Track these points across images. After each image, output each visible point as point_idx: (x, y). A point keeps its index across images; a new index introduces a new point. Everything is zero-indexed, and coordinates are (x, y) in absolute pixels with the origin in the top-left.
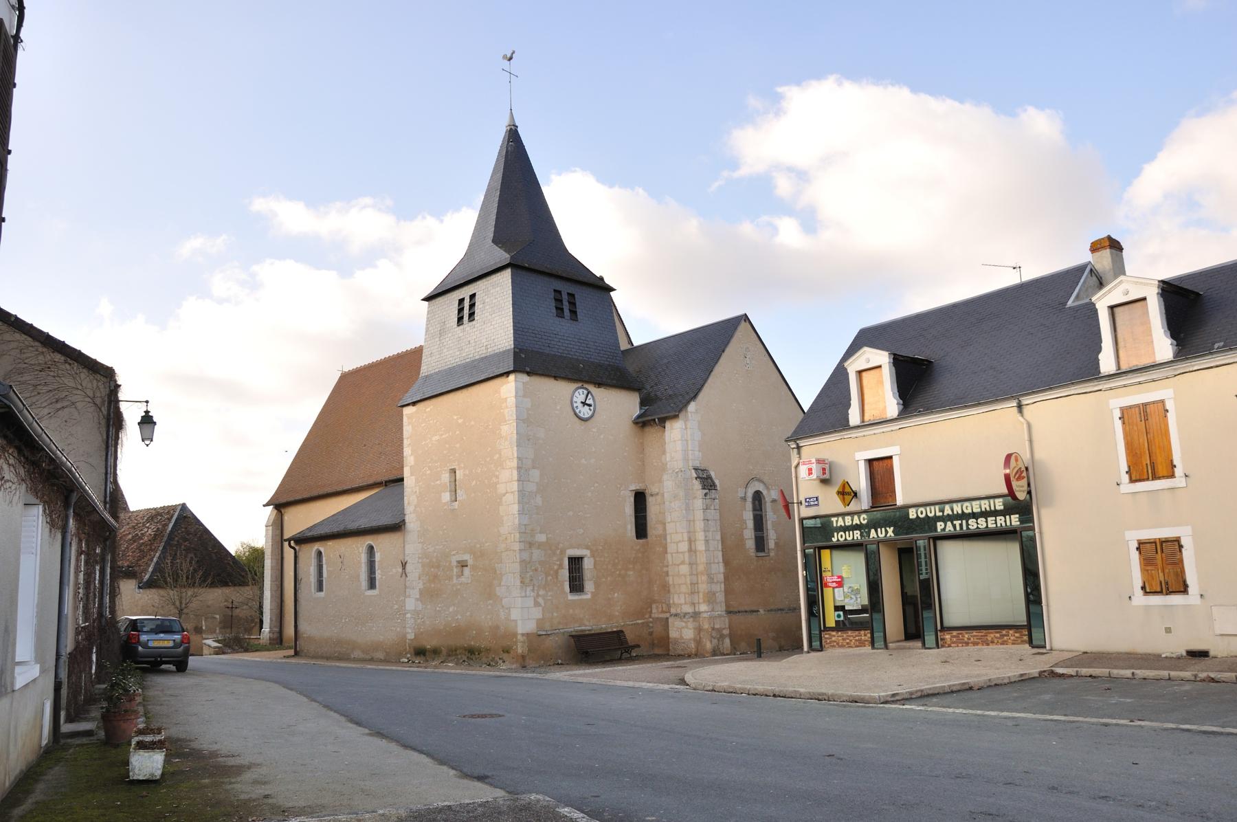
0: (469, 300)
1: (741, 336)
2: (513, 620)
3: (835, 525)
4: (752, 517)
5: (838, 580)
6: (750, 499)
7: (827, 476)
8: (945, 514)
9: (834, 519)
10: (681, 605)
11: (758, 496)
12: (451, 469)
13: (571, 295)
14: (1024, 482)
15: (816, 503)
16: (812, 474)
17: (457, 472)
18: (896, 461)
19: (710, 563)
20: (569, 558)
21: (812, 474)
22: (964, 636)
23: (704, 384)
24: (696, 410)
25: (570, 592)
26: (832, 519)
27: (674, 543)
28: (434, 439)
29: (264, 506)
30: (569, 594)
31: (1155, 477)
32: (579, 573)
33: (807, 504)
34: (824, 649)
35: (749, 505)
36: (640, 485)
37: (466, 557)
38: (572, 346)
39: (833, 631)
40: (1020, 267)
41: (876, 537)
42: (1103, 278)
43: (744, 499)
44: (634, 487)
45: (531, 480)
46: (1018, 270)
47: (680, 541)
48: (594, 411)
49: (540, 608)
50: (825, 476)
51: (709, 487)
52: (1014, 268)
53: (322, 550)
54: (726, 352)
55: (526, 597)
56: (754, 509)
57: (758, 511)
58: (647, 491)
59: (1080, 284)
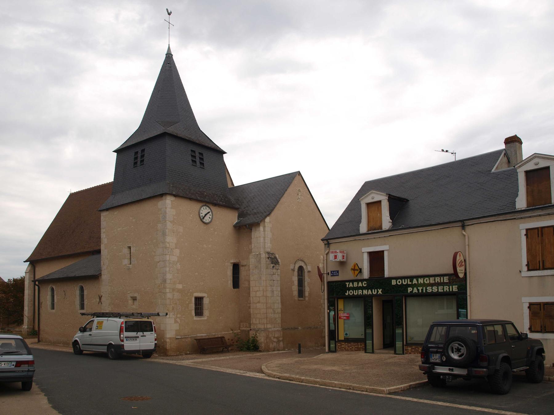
0: (140, 153)
1: (296, 183)
2: (162, 330)
3: (347, 286)
4: (297, 279)
5: (347, 315)
6: (296, 270)
7: (344, 260)
8: (413, 283)
9: (347, 284)
10: (257, 324)
11: (301, 269)
12: (128, 247)
13: (201, 154)
14: (463, 268)
15: (337, 274)
16: (336, 258)
17: (131, 248)
18: (386, 254)
19: (274, 303)
20: (195, 298)
21: (336, 258)
22: (419, 349)
23: (275, 207)
24: (270, 221)
25: (195, 316)
26: (346, 283)
27: (254, 291)
28: (119, 229)
29: (24, 262)
30: (194, 317)
31: (544, 269)
32: (200, 306)
33: (332, 274)
34: (337, 351)
35: (296, 273)
36: (237, 260)
37: (136, 295)
38: (200, 182)
39: (343, 342)
40: (455, 153)
41: (371, 294)
42: (510, 159)
43: (293, 270)
44: (233, 261)
45: (174, 254)
46: (454, 154)
47: (257, 291)
48: (212, 219)
49: (178, 324)
50: (344, 260)
51: (275, 263)
52: (452, 153)
53: (54, 287)
54: (287, 191)
55: (170, 318)
56: (298, 275)
57: (300, 276)
58: (240, 263)
59: (499, 161)
